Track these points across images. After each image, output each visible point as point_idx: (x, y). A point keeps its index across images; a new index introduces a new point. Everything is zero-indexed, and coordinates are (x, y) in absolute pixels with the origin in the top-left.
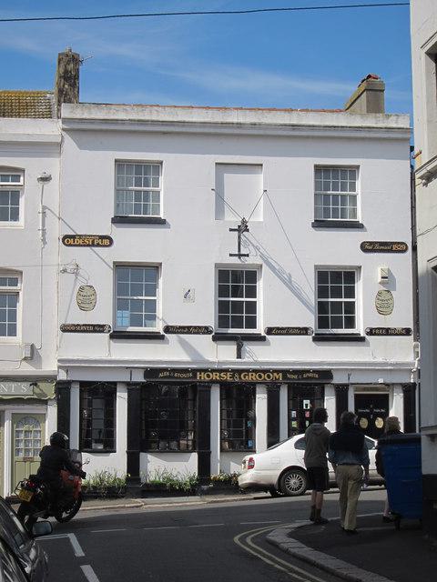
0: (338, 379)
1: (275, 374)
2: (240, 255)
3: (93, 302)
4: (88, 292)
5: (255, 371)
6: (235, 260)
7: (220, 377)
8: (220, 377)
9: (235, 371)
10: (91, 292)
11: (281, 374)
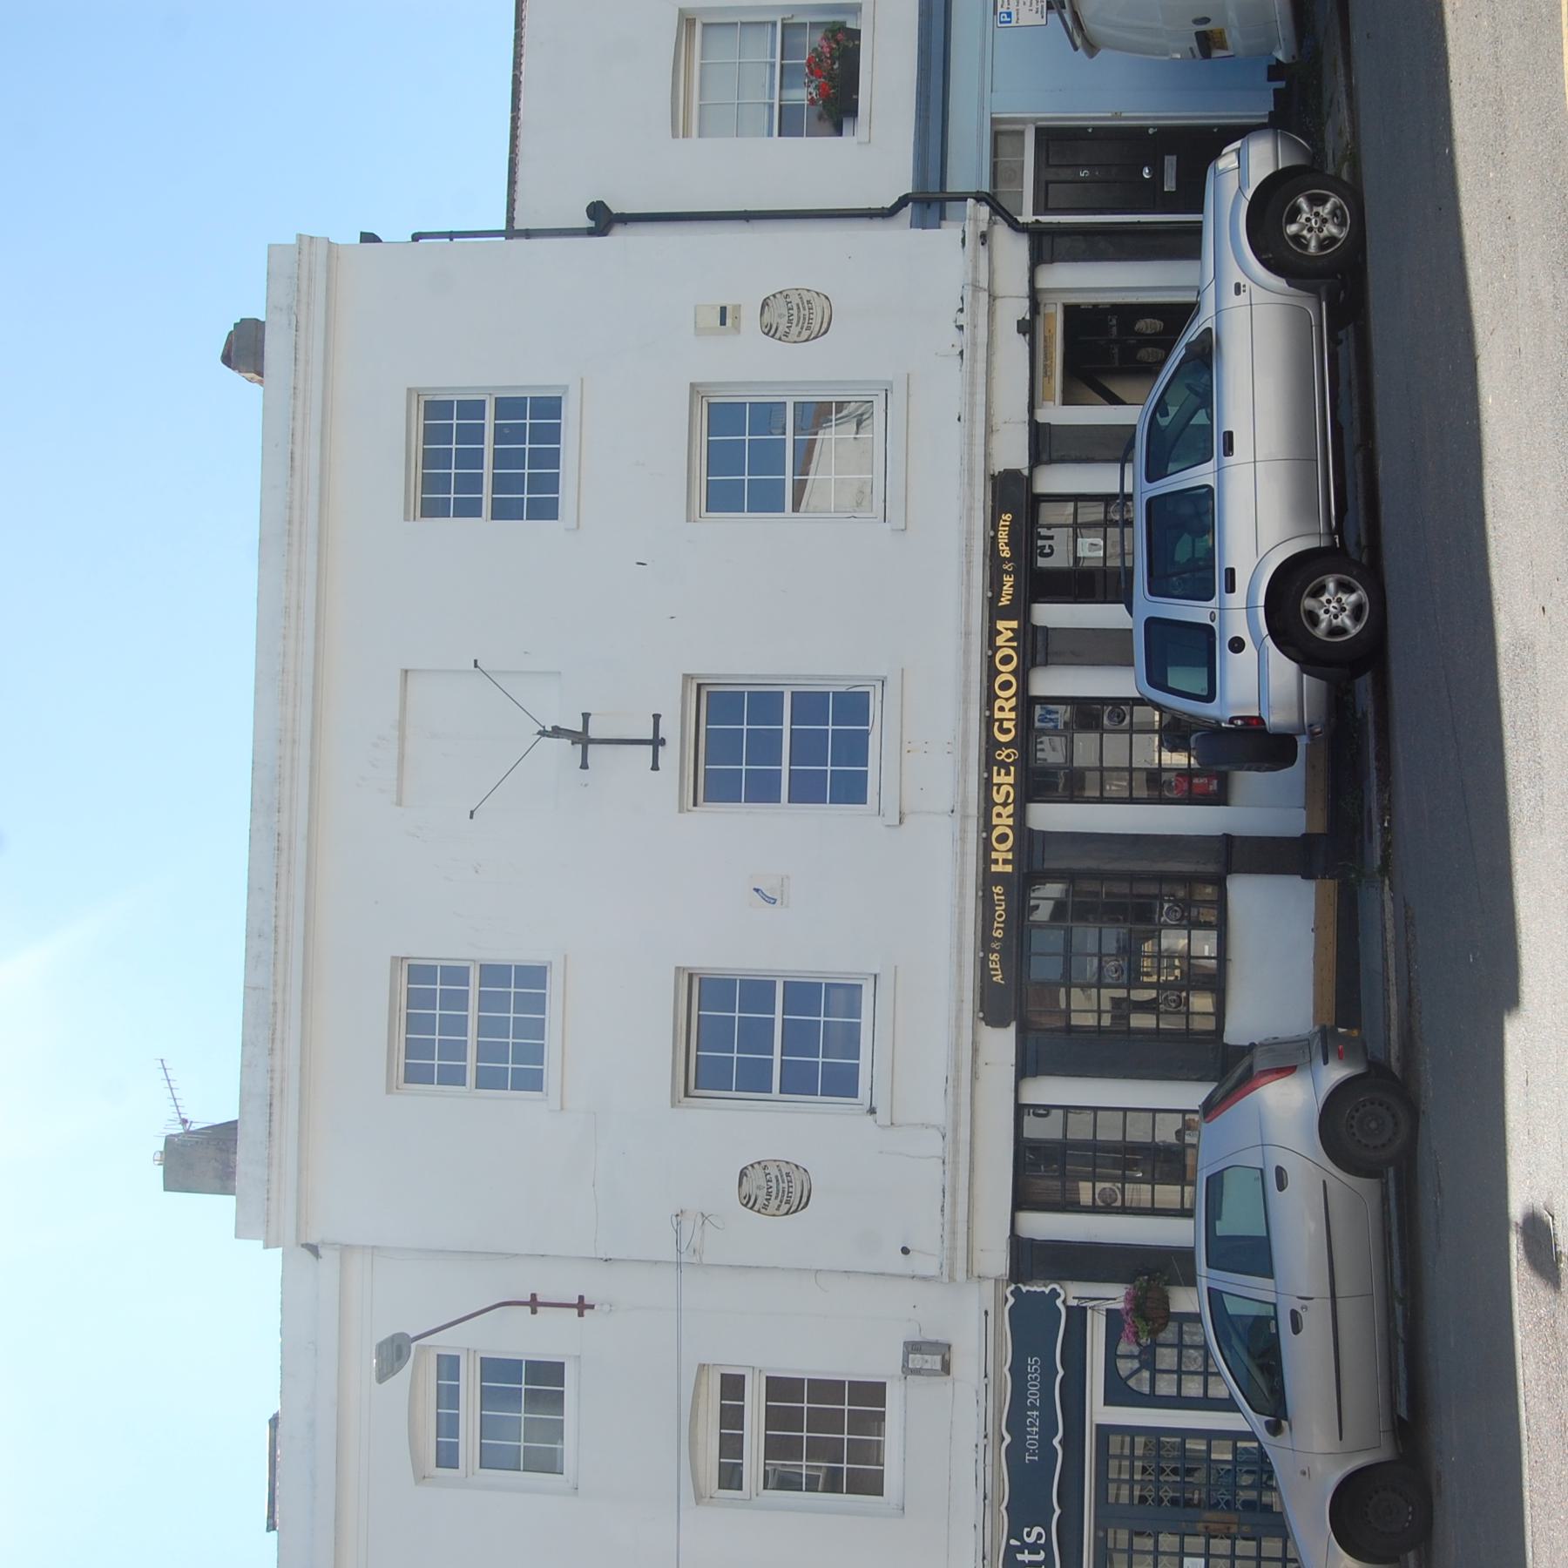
0: (1013, 453)
1: (1000, 641)
2: (657, 742)
3: (806, 296)
4: (756, 1179)
5: (990, 698)
6: (669, 755)
7: (1005, 804)
8: (1005, 804)
9: (989, 761)
10: (779, 306)
11: (1001, 625)
